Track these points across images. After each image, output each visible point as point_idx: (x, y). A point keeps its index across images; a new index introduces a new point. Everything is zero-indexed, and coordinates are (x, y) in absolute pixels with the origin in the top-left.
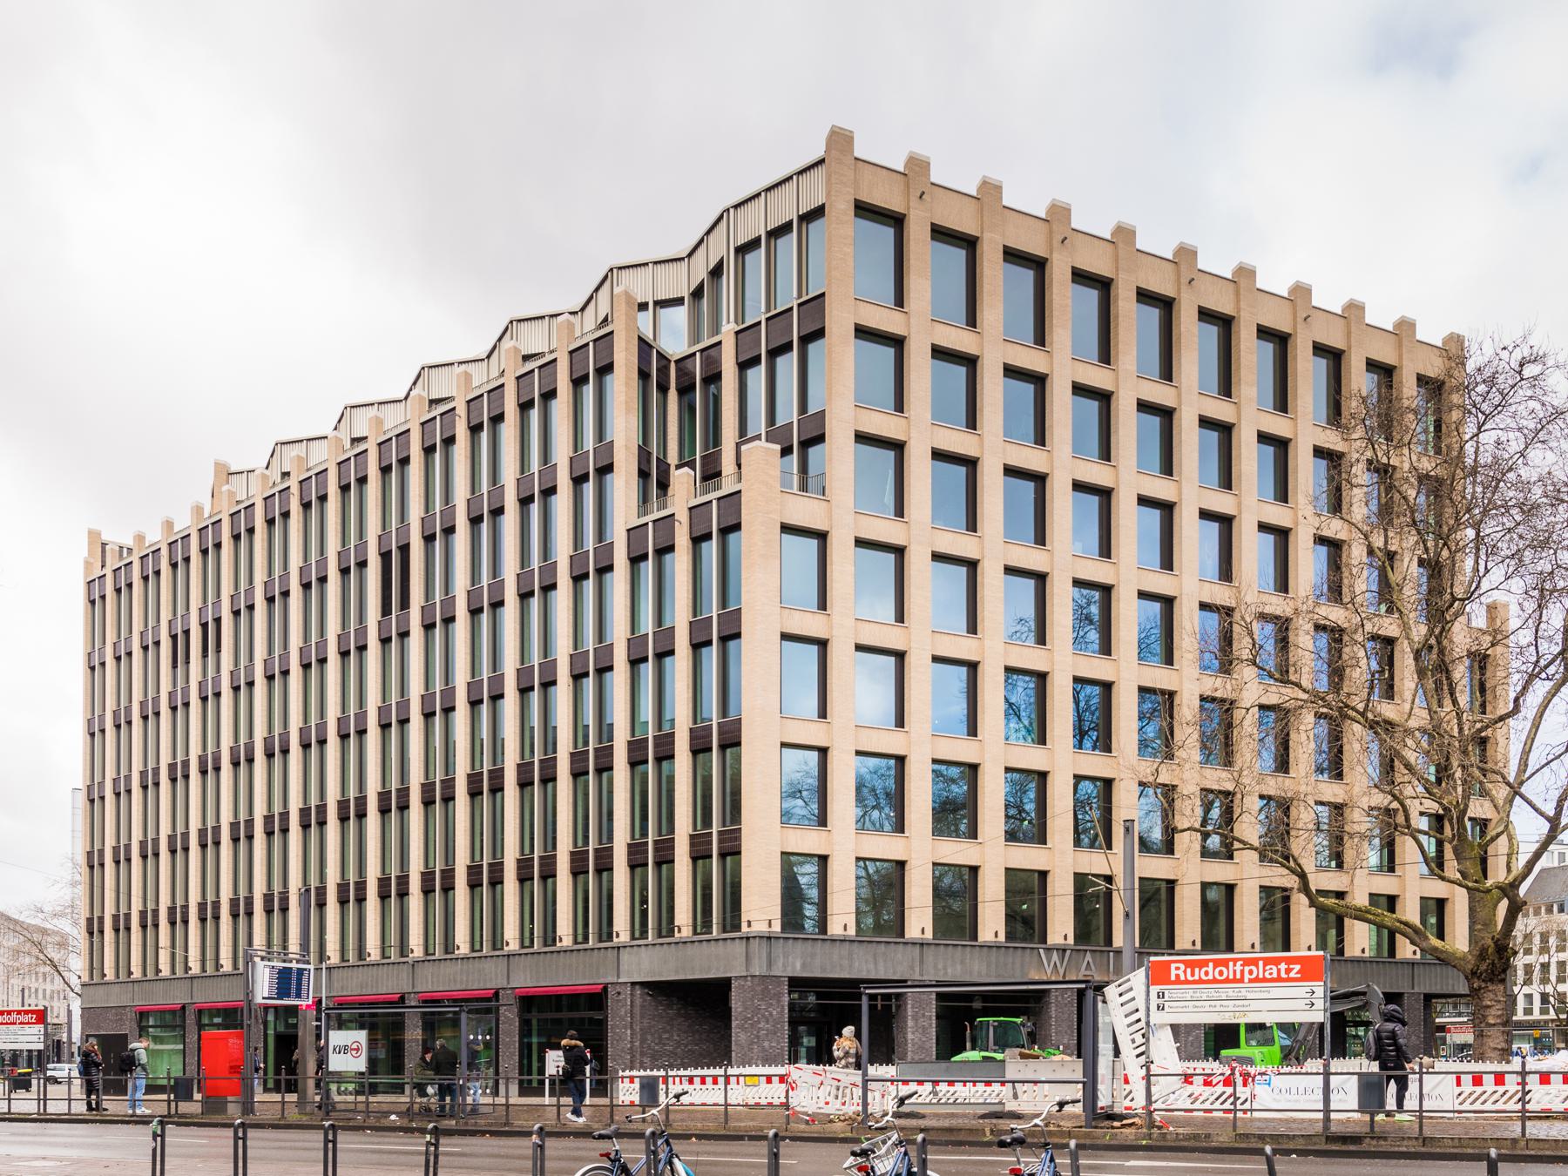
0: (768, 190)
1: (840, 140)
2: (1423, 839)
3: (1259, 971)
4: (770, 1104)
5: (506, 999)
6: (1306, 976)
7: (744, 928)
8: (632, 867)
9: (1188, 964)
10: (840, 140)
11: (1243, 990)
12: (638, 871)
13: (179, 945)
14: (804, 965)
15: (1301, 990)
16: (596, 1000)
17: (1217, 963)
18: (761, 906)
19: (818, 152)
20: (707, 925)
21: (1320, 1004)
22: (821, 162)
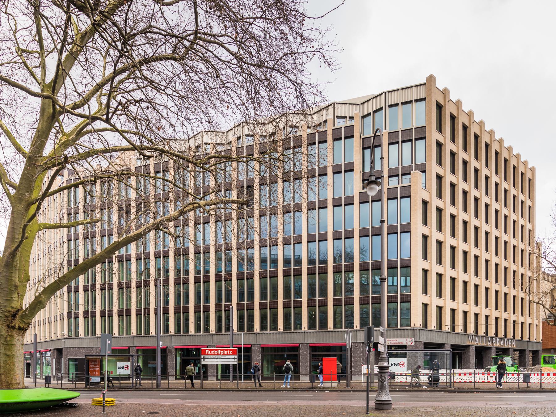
0: (373, 98)
1: (431, 79)
2: (546, 311)
3: (224, 352)
4: (465, 382)
5: (256, 348)
6: (233, 353)
7: (329, 329)
8: (85, 318)
9: (209, 350)
10: (431, 79)
11: (221, 356)
12: (103, 318)
13: (91, 330)
14: (427, 338)
15: (232, 356)
16: (295, 349)
17: (216, 350)
18: (416, 320)
19: (424, 81)
20: (179, 331)
21: (236, 360)
22: (425, 84)
